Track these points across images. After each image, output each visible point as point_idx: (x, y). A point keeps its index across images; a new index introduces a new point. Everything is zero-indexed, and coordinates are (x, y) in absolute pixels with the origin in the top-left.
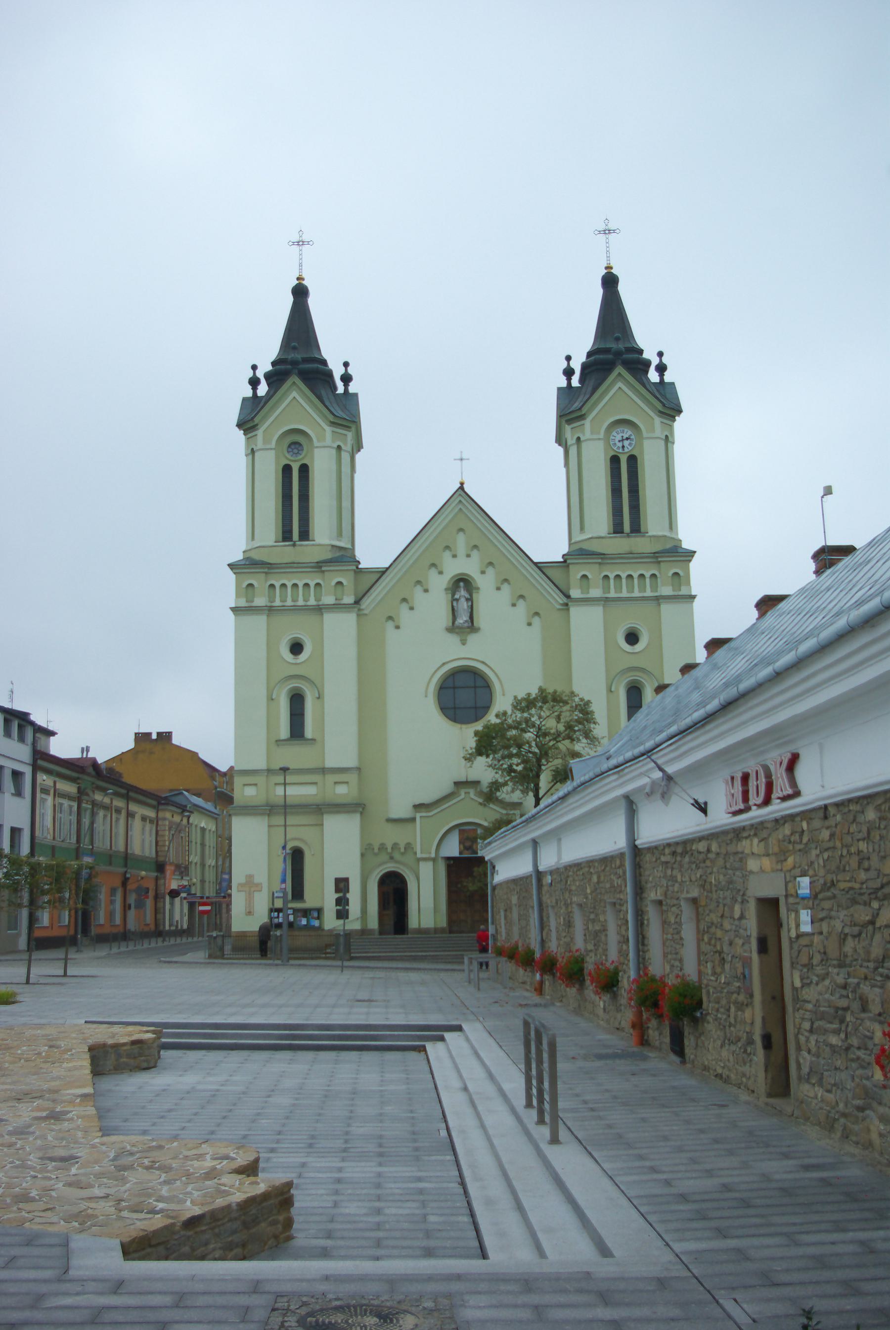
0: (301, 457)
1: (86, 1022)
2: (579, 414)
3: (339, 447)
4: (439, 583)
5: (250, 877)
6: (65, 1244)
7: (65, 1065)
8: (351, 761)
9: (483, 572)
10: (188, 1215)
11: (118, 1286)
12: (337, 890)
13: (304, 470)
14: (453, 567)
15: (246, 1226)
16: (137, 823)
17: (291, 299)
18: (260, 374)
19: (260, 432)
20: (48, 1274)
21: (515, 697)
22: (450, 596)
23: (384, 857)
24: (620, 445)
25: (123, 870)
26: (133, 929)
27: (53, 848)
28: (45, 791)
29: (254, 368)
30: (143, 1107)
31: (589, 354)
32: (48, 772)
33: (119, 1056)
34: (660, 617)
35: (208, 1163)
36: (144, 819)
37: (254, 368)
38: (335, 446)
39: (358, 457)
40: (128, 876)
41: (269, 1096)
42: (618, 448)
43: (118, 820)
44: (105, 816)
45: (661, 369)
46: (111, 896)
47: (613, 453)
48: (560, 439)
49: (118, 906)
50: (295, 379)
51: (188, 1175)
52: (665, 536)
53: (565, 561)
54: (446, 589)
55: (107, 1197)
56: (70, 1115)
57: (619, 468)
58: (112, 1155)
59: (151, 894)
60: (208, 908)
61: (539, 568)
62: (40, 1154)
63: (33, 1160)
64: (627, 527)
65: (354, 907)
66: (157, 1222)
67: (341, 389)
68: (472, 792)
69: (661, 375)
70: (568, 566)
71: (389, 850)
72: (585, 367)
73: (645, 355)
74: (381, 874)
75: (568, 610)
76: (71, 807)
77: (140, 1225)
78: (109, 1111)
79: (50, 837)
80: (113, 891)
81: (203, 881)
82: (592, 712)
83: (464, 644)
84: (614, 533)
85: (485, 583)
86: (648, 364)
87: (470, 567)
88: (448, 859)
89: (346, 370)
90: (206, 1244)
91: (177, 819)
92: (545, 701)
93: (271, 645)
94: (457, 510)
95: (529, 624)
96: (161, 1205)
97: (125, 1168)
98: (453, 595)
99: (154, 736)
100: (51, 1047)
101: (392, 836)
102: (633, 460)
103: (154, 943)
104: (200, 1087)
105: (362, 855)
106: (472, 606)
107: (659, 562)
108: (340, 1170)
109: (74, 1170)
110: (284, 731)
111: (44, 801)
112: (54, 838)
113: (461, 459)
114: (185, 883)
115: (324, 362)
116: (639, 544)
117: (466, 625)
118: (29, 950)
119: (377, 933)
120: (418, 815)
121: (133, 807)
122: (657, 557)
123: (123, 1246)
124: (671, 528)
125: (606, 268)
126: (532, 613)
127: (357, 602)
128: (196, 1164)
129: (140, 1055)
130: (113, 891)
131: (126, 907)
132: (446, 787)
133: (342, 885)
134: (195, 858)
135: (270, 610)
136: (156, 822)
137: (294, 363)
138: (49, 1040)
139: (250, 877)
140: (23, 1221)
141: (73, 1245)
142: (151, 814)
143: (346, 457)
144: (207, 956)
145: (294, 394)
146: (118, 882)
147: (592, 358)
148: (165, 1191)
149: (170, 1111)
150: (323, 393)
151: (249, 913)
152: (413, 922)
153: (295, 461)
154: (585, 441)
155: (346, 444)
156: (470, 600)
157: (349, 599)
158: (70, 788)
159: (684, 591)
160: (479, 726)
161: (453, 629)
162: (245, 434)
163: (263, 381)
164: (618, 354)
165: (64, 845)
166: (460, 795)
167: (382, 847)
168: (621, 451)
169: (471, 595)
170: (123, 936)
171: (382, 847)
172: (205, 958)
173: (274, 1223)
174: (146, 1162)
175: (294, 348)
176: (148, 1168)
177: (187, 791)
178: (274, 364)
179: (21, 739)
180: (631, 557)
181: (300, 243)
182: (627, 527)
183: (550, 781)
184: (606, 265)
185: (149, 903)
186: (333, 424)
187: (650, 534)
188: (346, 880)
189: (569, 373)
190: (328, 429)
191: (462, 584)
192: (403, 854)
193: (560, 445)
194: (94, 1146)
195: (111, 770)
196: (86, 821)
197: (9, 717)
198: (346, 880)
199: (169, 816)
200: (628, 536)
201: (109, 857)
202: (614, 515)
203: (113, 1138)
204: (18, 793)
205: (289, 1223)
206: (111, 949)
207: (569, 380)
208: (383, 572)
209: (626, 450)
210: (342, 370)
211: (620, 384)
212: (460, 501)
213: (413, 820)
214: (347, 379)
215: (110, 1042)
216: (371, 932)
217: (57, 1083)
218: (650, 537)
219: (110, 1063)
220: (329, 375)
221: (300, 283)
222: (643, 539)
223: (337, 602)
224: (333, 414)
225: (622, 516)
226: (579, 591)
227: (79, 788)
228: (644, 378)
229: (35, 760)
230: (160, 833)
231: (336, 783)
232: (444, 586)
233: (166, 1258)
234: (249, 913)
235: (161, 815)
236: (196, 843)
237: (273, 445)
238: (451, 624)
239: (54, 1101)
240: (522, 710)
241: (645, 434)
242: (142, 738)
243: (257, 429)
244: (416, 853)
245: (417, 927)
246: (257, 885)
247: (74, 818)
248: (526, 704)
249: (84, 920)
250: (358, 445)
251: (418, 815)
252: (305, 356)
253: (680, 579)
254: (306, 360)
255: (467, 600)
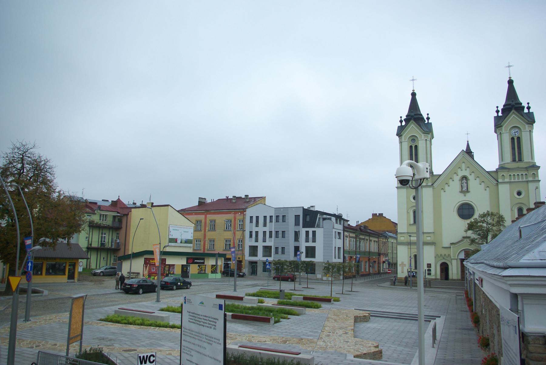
0: (415, 143)
1: (355, 309)
2: (500, 125)
3: (426, 139)
4: (457, 178)
5: (402, 263)
6: (346, 355)
7: (349, 321)
8: (431, 230)
9: (471, 175)
10: (364, 353)
11: (352, 361)
12: (428, 267)
13: (416, 147)
14: (461, 174)
15: (374, 355)
16: (372, 243)
17: (411, 97)
18: (403, 119)
19: (403, 137)
20: (343, 358)
21: (480, 214)
22: (461, 182)
23: (441, 258)
24: (514, 134)
25: (368, 256)
26: (372, 272)
27: (349, 252)
28: (347, 237)
29: (401, 117)
30: (364, 331)
31: (504, 106)
32: (347, 231)
33: (361, 319)
34: (528, 187)
35: (370, 345)
36: (374, 241)
37: (401, 117)
38: (425, 139)
39: (433, 140)
40: (370, 258)
41: (390, 331)
42: (514, 135)
43: (367, 242)
44: (363, 242)
45: (529, 108)
46: (365, 263)
47: (512, 137)
48: (496, 132)
49: (367, 266)
50: (412, 121)
51: (366, 346)
52: (530, 162)
53: (497, 171)
54: (459, 180)
55: (353, 349)
56: (349, 333)
57: (514, 141)
58: (355, 342)
59: (377, 263)
60: (390, 272)
61: (488, 173)
62: (343, 340)
63: (342, 341)
64: (517, 159)
65: (433, 272)
66: (359, 353)
67: (426, 122)
68: (468, 240)
69: (529, 110)
70: (498, 172)
71: (443, 256)
72: (502, 110)
73: (523, 105)
74: (441, 262)
75: (498, 185)
76: (354, 240)
77: (357, 353)
78: (357, 331)
79: (348, 249)
80: (366, 262)
81: (392, 258)
82: (504, 218)
83: (465, 196)
84: (513, 161)
85: (471, 178)
86: (523, 107)
87: (466, 173)
88: (461, 259)
89: (428, 116)
90: (367, 357)
91: (384, 240)
92: (489, 215)
93: (408, 198)
94: (462, 157)
95: (486, 190)
96: (361, 351)
97: (356, 344)
98: (461, 182)
99: (378, 215)
100: (347, 316)
101: (446, 252)
102: (519, 138)
103: (377, 277)
104: (376, 327)
105: (435, 257)
106: (467, 185)
107: (528, 170)
108: (396, 348)
109: (348, 344)
110: (412, 222)
111: (346, 239)
112: (349, 249)
113: (467, 134)
114: (387, 259)
115: (421, 115)
116: (521, 165)
117: (466, 190)
118: (343, 279)
119: (440, 279)
120: (452, 246)
121: (371, 238)
122: (527, 169)
123: (354, 356)
124: (532, 159)
125: (509, 78)
126: (486, 186)
127: (432, 185)
128: (368, 345)
129: (365, 319)
130: (366, 262)
131: (370, 266)
132: (460, 238)
133: (429, 265)
134: (390, 251)
135: (510, 183)
136: (378, 242)
137: (412, 116)
138: (346, 314)
139: (402, 263)
140: (340, 351)
141: (347, 355)
142: (376, 240)
143: (428, 142)
144: (390, 284)
145: (412, 125)
146: (367, 260)
147: (505, 107)
148: (362, 349)
149: (369, 332)
150: (421, 124)
151: (403, 272)
152: (450, 277)
153: (413, 144)
154: (503, 133)
155: (428, 139)
156: (467, 183)
157: (430, 184)
158: (353, 235)
159: (536, 179)
160: (472, 220)
161: (462, 192)
162: (399, 137)
163: (404, 122)
164: (513, 106)
165: (352, 251)
166: (464, 241)
167: (441, 255)
168: (514, 136)
169: (467, 182)
170: (368, 275)
171: (441, 255)
172: (389, 285)
173: (379, 356)
174: (360, 344)
175: (412, 112)
176: (360, 345)
177: (387, 232)
178: (406, 116)
179: (340, 224)
180: (518, 169)
181: (413, 80)
182: (517, 159)
183: (491, 238)
184: (509, 77)
185: (376, 265)
186: (424, 133)
187: (525, 161)
188: (430, 264)
189: (497, 112)
190: (423, 135)
191: (464, 178)
192: (447, 257)
193: (496, 133)
194: (352, 340)
195: (365, 227)
196: (358, 243)
197: (337, 218)
198: (430, 264)
199: (382, 240)
200: (517, 162)
201: (365, 253)
202: (512, 156)
203: (356, 339)
204: (340, 238)
205: (381, 356)
206: (365, 280)
207: (498, 114)
208: (440, 175)
209: (516, 135)
210: (427, 116)
211: (514, 115)
212: (463, 154)
213: (450, 247)
214: (428, 118)
215: (359, 315)
216: (438, 279)
217: (347, 326)
218: (525, 162)
219: (359, 320)
220: (423, 118)
221: (413, 92)
222: (522, 163)
223: (426, 185)
224: (424, 131)
225: (515, 156)
226: (501, 180)
227: (356, 235)
228: (522, 113)
229: (344, 229)
230: (379, 245)
231: (427, 237)
232: (459, 179)
233: (361, 358)
234: (403, 272)
235: (379, 239)
236: (390, 247)
237: (508, 132)
238: (461, 190)
239: (346, 330)
240: (482, 218)
241: (522, 130)
242: (374, 215)
243: (502, 127)
244: (451, 257)
245: (451, 278)
246: (405, 265)
247: (355, 243)
248: (484, 216)
249: (358, 272)
250: (433, 137)
251: (452, 246)
252: (415, 113)
253: (535, 175)
254: (415, 115)
255: (466, 183)
